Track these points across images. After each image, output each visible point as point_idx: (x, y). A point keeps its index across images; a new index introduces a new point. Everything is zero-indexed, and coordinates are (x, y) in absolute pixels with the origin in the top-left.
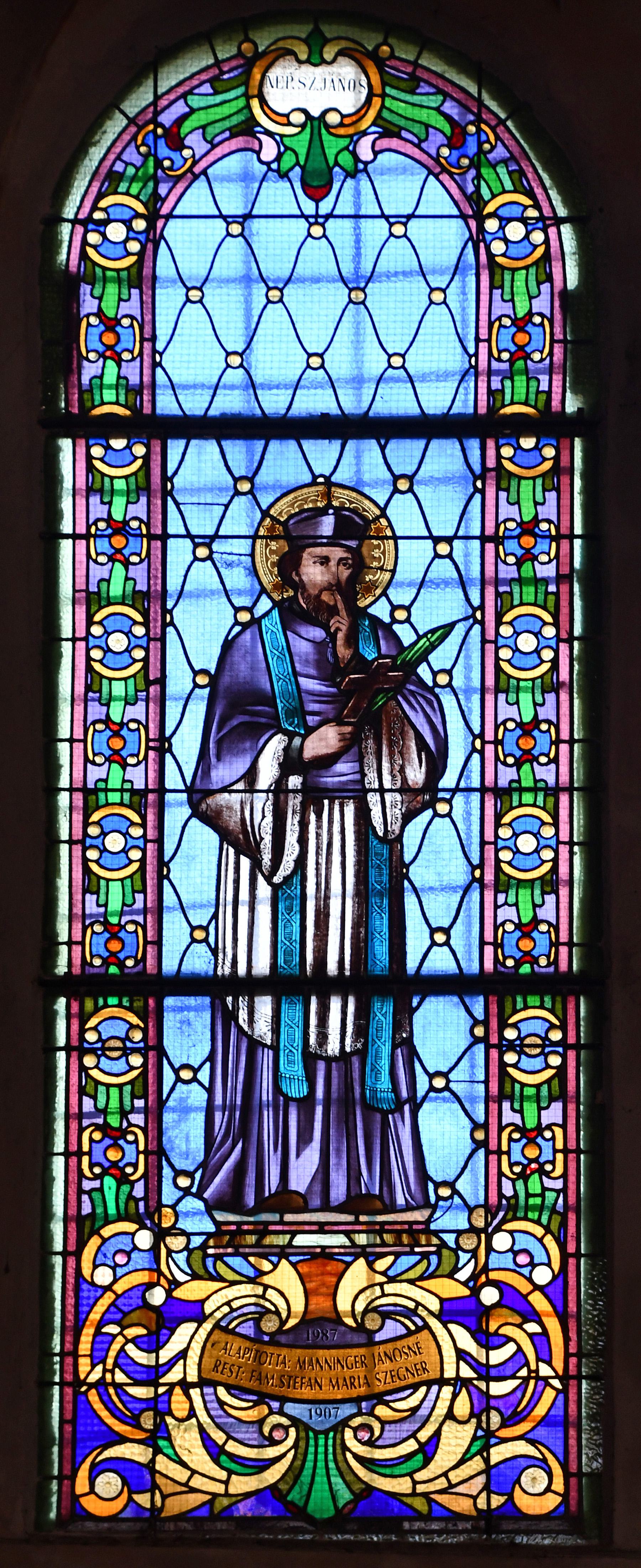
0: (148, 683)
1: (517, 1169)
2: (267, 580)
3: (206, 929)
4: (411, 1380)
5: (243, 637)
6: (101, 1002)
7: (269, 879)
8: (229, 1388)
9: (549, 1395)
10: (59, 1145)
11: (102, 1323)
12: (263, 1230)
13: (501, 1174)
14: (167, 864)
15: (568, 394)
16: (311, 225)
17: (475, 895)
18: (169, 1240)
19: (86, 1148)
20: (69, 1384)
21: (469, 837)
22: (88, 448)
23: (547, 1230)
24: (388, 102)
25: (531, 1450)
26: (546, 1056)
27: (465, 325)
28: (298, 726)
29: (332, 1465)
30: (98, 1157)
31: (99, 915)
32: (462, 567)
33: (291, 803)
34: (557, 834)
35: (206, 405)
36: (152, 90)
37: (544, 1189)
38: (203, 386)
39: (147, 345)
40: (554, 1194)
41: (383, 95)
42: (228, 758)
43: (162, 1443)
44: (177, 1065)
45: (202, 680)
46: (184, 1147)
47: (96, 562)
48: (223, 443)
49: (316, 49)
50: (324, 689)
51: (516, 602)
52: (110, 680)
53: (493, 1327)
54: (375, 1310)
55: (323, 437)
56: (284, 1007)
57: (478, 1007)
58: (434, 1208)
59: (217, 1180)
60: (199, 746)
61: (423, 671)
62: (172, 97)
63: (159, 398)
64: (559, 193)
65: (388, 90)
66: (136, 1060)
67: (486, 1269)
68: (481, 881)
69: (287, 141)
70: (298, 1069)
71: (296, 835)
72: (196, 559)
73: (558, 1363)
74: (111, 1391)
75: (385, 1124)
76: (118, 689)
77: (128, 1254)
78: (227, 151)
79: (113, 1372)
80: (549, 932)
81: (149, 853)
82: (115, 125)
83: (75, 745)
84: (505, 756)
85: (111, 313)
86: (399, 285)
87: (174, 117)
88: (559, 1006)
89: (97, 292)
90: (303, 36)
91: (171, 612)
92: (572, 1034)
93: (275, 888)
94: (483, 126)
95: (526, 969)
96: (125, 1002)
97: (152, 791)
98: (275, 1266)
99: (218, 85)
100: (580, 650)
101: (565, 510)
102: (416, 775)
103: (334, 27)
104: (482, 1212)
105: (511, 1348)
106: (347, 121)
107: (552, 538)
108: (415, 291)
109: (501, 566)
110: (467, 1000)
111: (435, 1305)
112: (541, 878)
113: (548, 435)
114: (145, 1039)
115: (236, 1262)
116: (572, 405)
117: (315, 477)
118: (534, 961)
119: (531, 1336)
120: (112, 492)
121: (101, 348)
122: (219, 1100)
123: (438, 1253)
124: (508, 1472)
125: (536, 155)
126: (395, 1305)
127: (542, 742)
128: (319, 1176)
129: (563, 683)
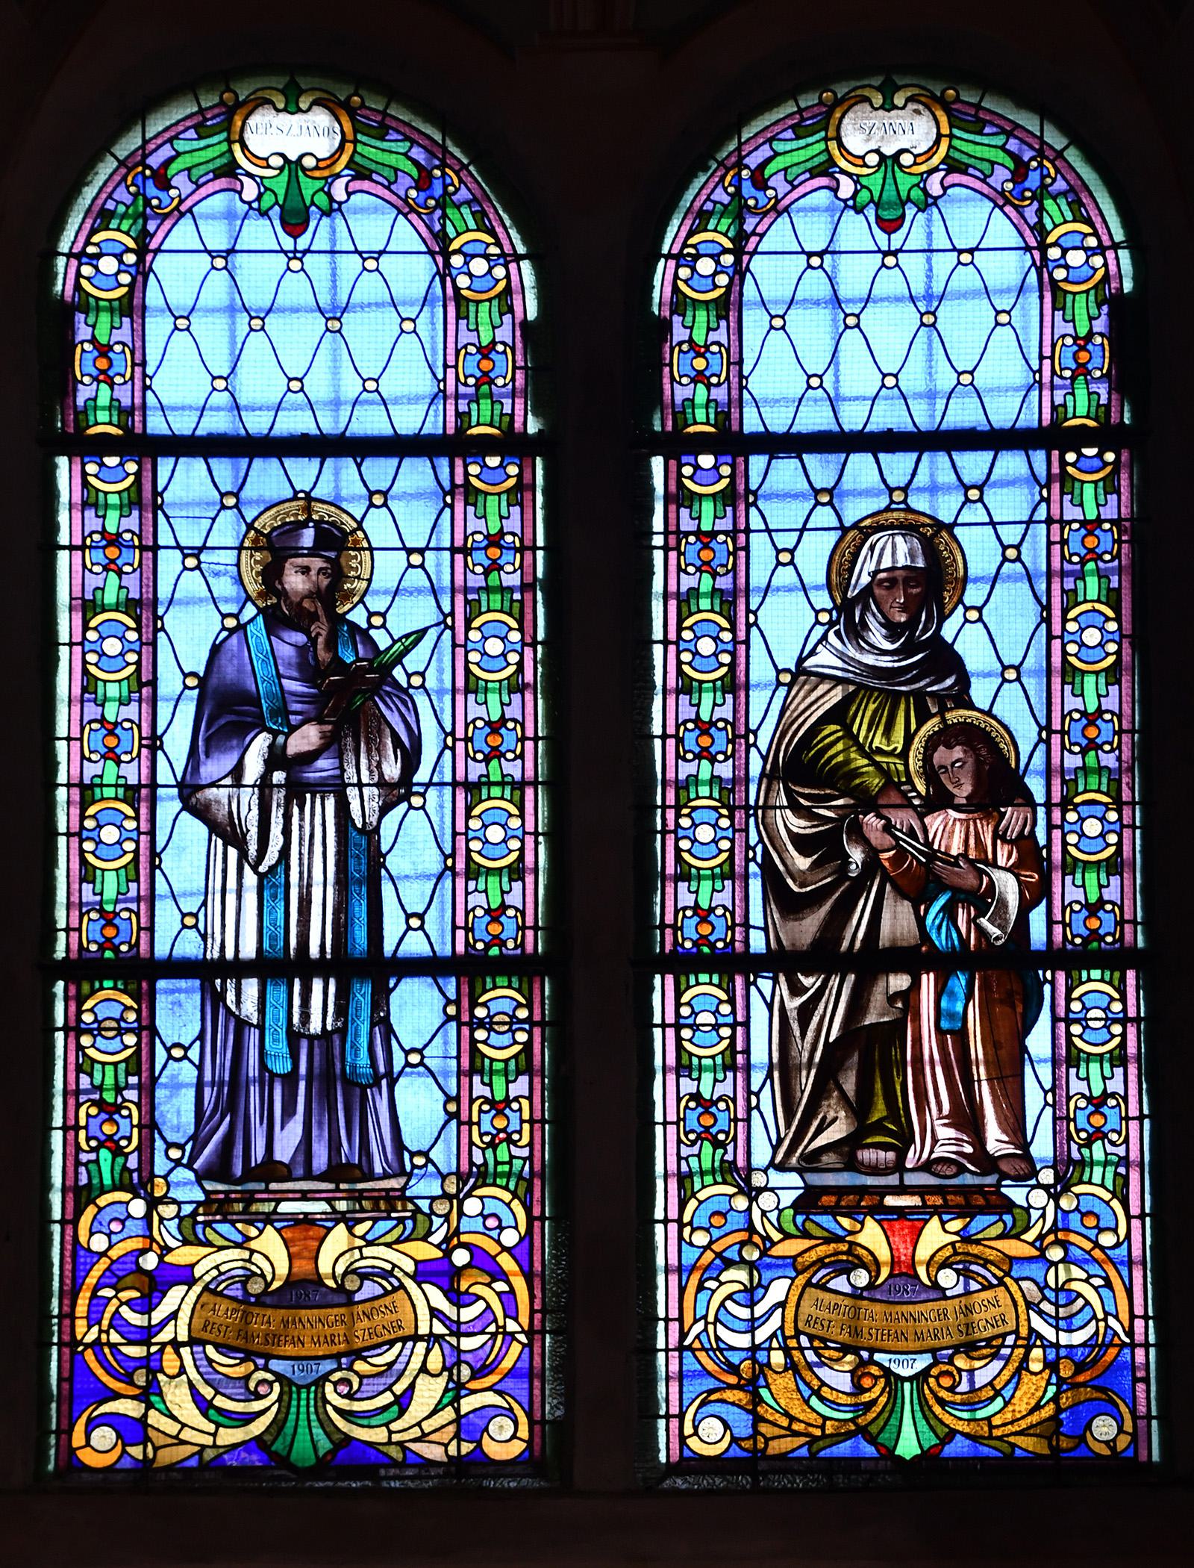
0: (141, 685)
1: (487, 1139)
2: (253, 588)
3: (195, 915)
4: (387, 1337)
5: (229, 641)
6: (97, 985)
7: (255, 868)
8: (217, 1347)
9: (515, 1349)
10: (58, 1120)
11: (98, 1287)
12: (249, 1198)
13: (471, 1143)
14: (159, 855)
15: (530, 416)
16: (290, 259)
17: (448, 883)
18: (160, 1208)
19: (82, 1122)
20: (66, 1345)
21: (442, 828)
22: (83, 465)
23: (515, 1195)
24: (360, 147)
25: (498, 1400)
26: (514, 1032)
27: (434, 350)
28: (281, 725)
29: (313, 1417)
30: (94, 1130)
31: (95, 903)
32: (433, 577)
33: (275, 797)
34: (523, 825)
35: (194, 425)
36: (140, 135)
37: (512, 1157)
38: (191, 408)
39: (138, 370)
40: (521, 1162)
41: (355, 142)
42: (216, 755)
43: (154, 1399)
44: (169, 1045)
45: (192, 682)
46: (175, 1122)
47: (91, 571)
48: (210, 460)
49: (292, 99)
50: (306, 690)
51: (484, 609)
52: (105, 682)
53: (463, 1287)
54: (354, 1272)
55: (303, 456)
56: (269, 988)
57: (451, 987)
58: (410, 1176)
59: (207, 1151)
60: (189, 744)
61: (398, 673)
62: (159, 141)
63: (149, 419)
64: (518, 232)
65: (359, 137)
66: (130, 1040)
67: (457, 1232)
68: (453, 869)
69: (864, 181)
70: (283, 1047)
71: (281, 827)
72: (185, 568)
73: (524, 1319)
74: (107, 1350)
75: (364, 1099)
76: (113, 690)
77: (123, 1222)
78: (211, 191)
79: (107, 1332)
80: (516, 917)
81: (142, 845)
82: (106, 168)
83: (72, 743)
84: (475, 752)
85: (103, 340)
86: (372, 314)
87: (161, 160)
88: (525, 986)
89: (91, 321)
90: (281, 87)
91: (161, 618)
92: (537, 1011)
93: (261, 877)
94: (447, 170)
95: (494, 951)
96: (120, 985)
97: (145, 786)
98: (261, 1232)
99: (202, 131)
100: (543, 654)
101: (528, 523)
102: (392, 770)
103: (309, 79)
104: (453, 1179)
105: (480, 1306)
106: (322, 164)
107: (516, 550)
108: (387, 321)
109: (470, 575)
110: (440, 981)
111: (410, 1267)
112: (509, 866)
113: (512, 455)
114: (138, 1020)
115: (224, 1228)
116: (533, 427)
117: (296, 492)
118: (502, 944)
119: (499, 1294)
120: (106, 506)
121: (95, 373)
122: (208, 1077)
123: (413, 1218)
124: (477, 1421)
125: (496, 196)
126: (373, 1267)
127: (509, 739)
128: (302, 1147)
129: (528, 684)
